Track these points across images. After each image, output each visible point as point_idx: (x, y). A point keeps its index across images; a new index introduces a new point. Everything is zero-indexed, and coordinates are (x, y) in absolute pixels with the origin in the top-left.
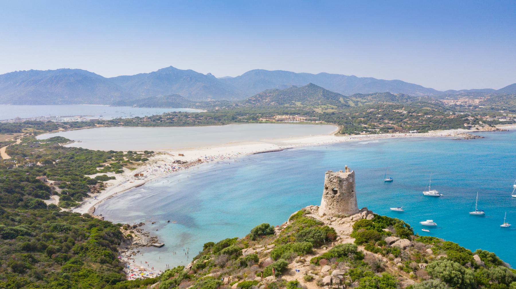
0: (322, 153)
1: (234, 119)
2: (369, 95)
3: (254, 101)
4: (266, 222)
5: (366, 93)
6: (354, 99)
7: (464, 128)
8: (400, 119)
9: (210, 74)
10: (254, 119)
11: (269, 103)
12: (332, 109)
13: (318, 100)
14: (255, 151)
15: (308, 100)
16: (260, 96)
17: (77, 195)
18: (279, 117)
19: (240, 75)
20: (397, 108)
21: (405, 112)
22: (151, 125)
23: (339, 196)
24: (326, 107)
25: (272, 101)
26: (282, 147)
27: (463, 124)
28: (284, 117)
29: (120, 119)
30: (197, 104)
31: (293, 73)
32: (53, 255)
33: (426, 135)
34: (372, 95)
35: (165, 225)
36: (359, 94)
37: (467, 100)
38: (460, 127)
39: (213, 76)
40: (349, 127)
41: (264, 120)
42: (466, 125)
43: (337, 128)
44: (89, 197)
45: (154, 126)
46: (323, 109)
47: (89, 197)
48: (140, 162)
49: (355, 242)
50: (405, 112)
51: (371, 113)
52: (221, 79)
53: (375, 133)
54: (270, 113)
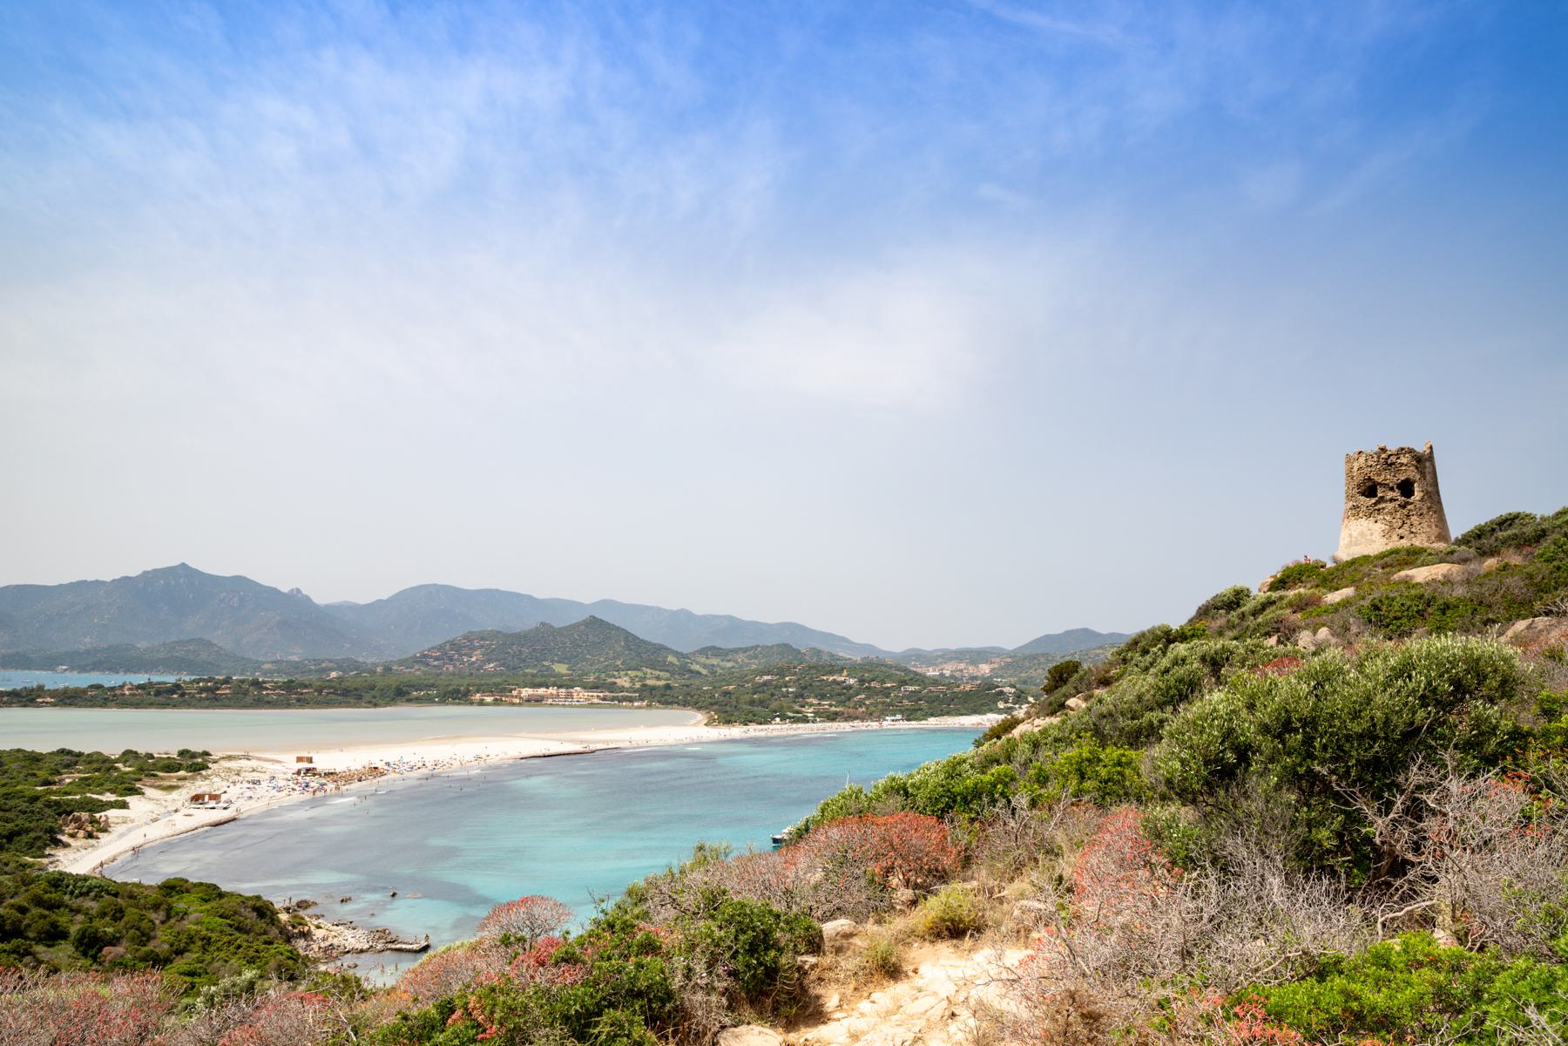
0: (708, 758)
1: (400, 694)
2: (736, 651)
3: (437, 659)
4: (1239, 585)
5: (731, 646)
6: (703, 660)
7: (1000, 711)
8: (843, 694)
9: (298, 591)
10: (457, 695)
11: (480, 667)
12: (658, 678)
13: (614, 658)
14: (526, 753)
15: (586, 660)
16: (454, 645)
17: (25, 838)
18: (527, 692)
19: (385, 597)
20: (831, 673)
21: (852, 681)
22: (151, 705)
23: (1422, 500)
24: (640, 674)
25: (489, 661)
26: (592, 747)
27: (996, 703)
28: (541, 691)
29: (41, 688)
30: (266, 666)
31: (530, 598)
32: (106, 950)
33: (923, 724)
34: (745, 650)
35: (385, 903)
36: (713, 648)
37: (962, 666)
38: (991, 711)
39: (308, 598)
40: (726, 709)
41: (489, 699)
42: (1001, 705)
43: (700, 716)
44: (66, 846)
45: (163, 706)
46: (632, 680)
47: (66, 846)
48: (182, 773)
49: (818, 997)
50: (852, 681)
51: (765, 684)
52: (328, 606)
53: (805, 720)
54: (496, 685)
